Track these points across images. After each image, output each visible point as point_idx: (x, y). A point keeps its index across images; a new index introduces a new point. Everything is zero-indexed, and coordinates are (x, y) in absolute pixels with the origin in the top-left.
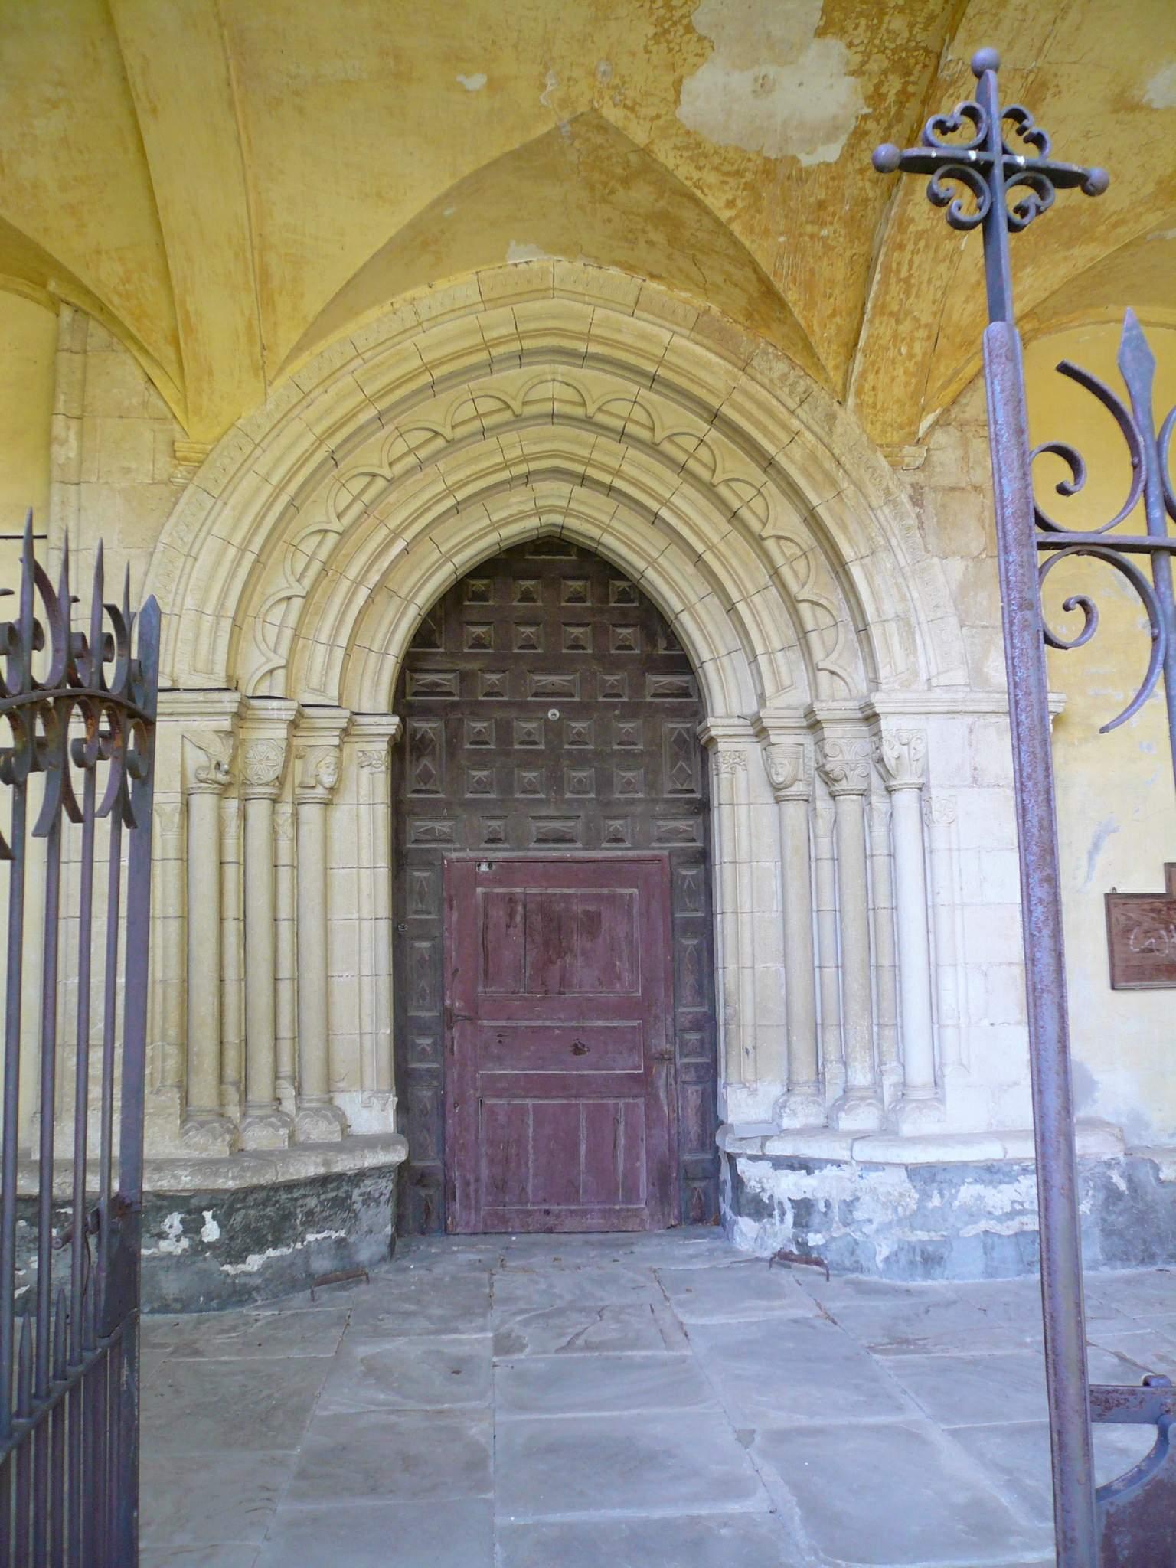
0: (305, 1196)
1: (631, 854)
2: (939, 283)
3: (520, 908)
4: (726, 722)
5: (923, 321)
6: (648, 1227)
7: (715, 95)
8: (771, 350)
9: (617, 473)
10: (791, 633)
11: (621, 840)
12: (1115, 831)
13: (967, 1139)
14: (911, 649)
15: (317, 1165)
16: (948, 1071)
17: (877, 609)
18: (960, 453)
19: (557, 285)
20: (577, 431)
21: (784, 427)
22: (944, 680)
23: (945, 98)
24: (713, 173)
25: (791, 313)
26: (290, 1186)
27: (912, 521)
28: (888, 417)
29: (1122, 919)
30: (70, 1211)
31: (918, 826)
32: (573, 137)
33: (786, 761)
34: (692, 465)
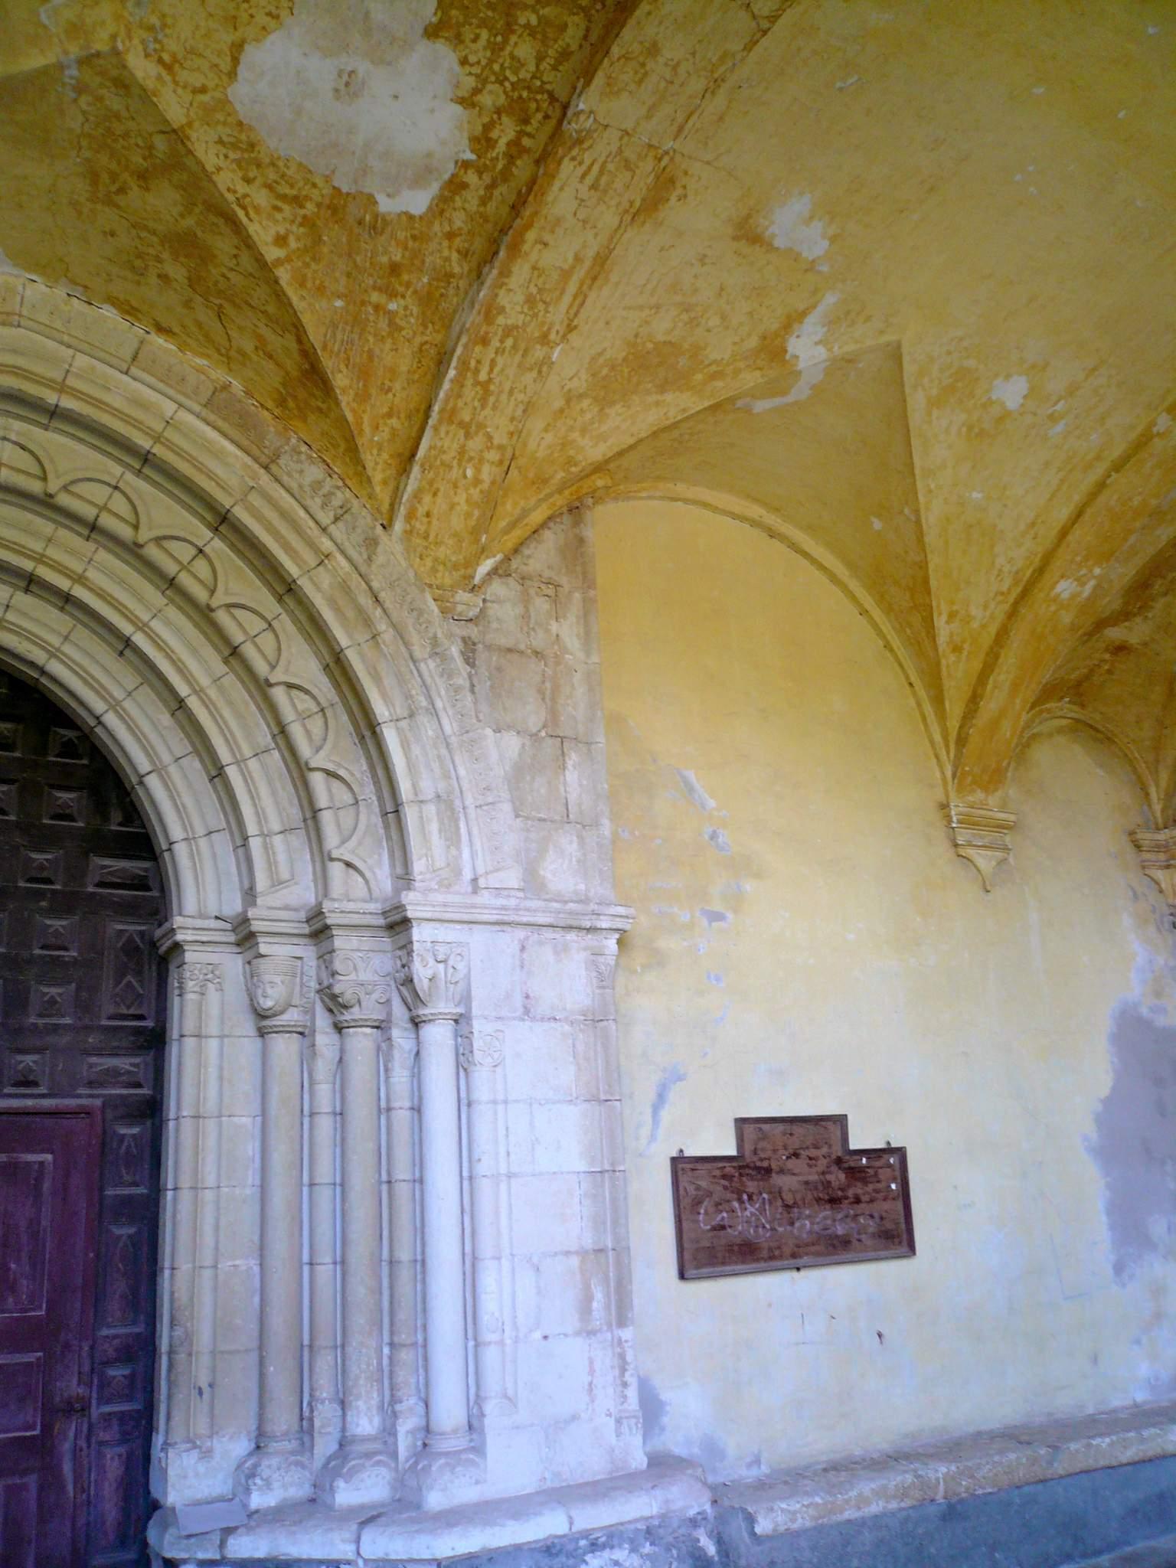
1: (48, 1103)
2: (521, 397)
4: (199, 923)
5: (496, 442)
7: (282, 79)
8: (304, 448)
9: (80, 579)
10: (295, 813)
11: (35, 1084)
12: (681, 1078)
13: (517, 1507)
14: (453, 839)
16: (489, 1408)
17: (414, 786)
18: (519, 610)
19: (25, 312)
20: (30, 516)
21: (311, 545)
22: (494, 881)
23: (566, 161)
24: (264, 191)
25: (338, 403)
27: (462, 681)
28: (442, 552)
29: (691, 1189)
31: (452, 1069)
32: (80, 89)
33: (278, 979)
34: (185, 579)
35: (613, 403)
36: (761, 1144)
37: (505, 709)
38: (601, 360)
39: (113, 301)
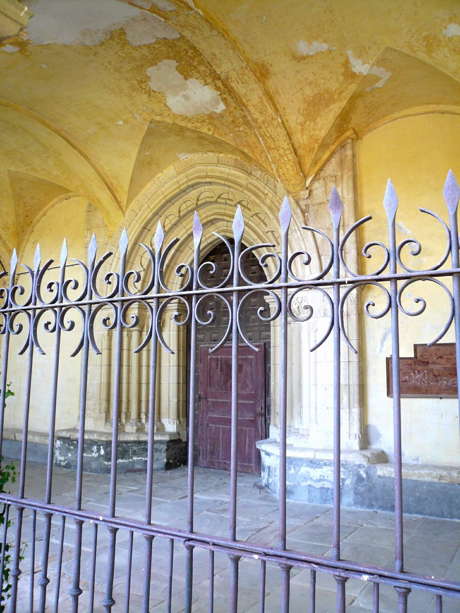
0: (132, 446)
3: (220, 363)
6: (254, 472)
8: (256, 167)
15: (134, 437)
18: (323, 189)
26: (127, 442)
28: (293, 182)
30: (75, 442)
35: (316, 118)
36: (425, 353)
37: (319, 223)
38: (301, 111)
39: (209, 151)
